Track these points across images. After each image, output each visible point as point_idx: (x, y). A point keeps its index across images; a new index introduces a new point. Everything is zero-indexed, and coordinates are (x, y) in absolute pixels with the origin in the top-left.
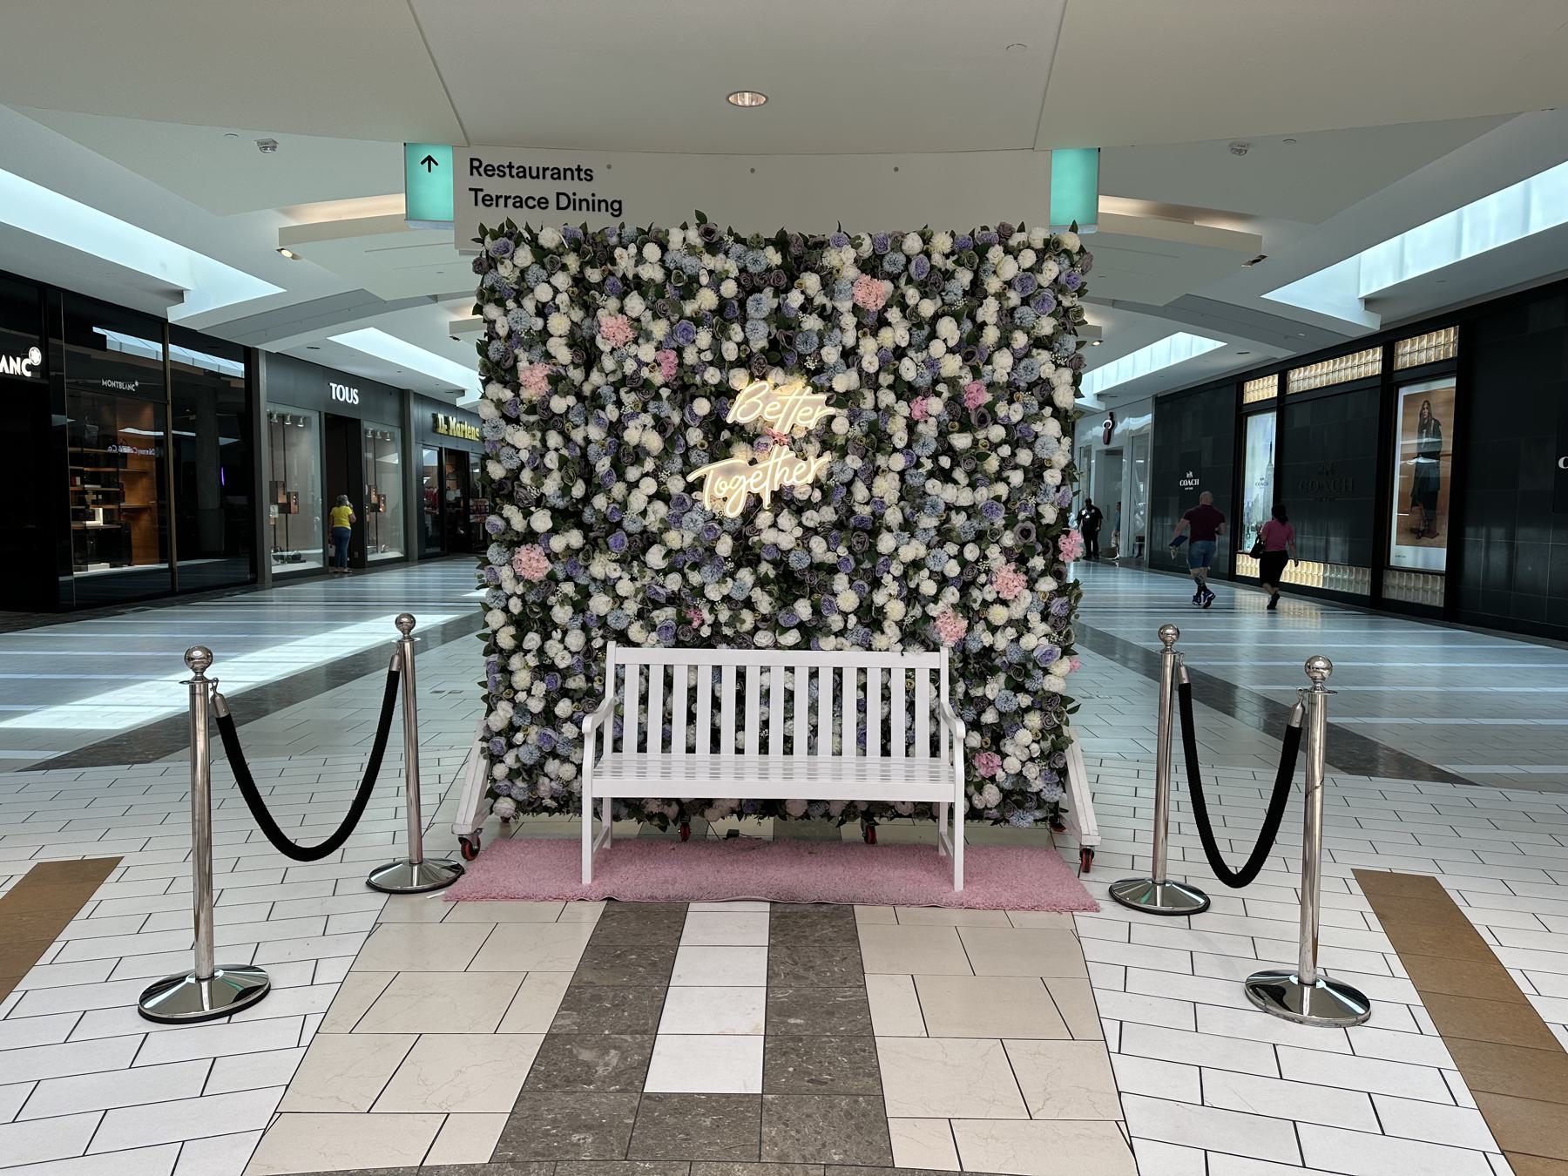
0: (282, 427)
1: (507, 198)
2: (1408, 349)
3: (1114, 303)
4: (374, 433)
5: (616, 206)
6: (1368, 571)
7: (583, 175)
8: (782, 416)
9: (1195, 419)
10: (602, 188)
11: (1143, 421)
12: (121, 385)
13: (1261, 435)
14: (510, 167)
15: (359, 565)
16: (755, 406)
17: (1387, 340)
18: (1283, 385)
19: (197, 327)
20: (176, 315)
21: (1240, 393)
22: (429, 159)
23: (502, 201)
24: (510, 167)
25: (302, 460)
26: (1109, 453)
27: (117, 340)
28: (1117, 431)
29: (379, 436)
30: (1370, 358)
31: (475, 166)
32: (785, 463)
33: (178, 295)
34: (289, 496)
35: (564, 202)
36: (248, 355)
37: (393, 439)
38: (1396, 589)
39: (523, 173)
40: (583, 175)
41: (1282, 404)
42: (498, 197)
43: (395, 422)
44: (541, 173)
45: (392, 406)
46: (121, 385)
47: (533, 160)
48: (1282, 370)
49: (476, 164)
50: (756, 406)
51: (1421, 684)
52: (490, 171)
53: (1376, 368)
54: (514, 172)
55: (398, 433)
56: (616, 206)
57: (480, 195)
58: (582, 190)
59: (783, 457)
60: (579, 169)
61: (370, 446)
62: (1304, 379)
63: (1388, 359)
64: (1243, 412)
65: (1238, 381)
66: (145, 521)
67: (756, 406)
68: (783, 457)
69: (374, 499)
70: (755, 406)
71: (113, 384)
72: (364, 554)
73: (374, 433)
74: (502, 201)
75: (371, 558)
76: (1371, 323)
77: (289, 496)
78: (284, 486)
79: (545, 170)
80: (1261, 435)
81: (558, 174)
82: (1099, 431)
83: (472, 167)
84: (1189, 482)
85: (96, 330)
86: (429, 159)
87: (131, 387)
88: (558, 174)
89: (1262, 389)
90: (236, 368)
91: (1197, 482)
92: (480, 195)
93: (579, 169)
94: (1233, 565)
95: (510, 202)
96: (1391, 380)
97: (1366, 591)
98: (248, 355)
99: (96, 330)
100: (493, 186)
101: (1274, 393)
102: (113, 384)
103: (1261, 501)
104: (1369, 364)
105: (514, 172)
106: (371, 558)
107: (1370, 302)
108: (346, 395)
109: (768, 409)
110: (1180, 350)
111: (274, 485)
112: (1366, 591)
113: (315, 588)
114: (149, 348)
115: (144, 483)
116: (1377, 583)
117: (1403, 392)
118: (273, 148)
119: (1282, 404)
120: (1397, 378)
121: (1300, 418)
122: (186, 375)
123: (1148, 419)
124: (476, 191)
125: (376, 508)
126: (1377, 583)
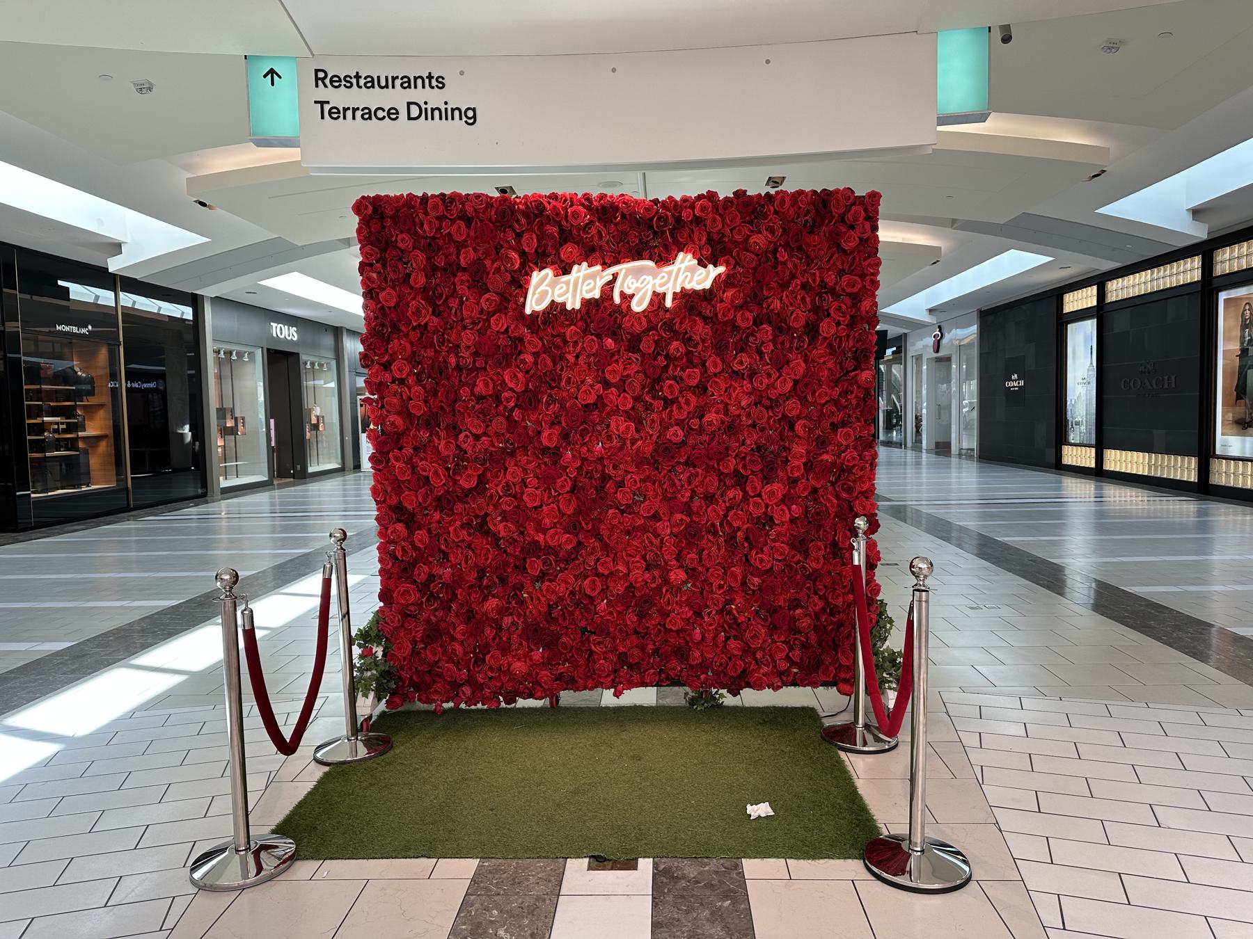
0: (228, 361)
1: (355, 110)
2: (1227, 256)
3: (953, 223)
4: (313, 364)
5: (470, 114)
6: (1194, 461)
7: (434, 83)
8: (570, 295)
9: (1019, 331)
10: (455, 96)
11: (971, 332)
12: (75, 330)
13: (1081, 343)
14: (358, 77)
15: (302, 476)
16: (545, 293)
17: (1206, 250)
18: (1101, 295)
19: (137, 276)
20: (115, 265)
21: (1060, 304)
22: (272, 72)
23: (349, 113)
24: (358, 77)
25: (252, 389)
26: (938, 360)
27: (79, 292)
28: (944, 341)
29: (317, 367)
30: (1189, 266)
31: (321, 77)
32: (687, 269)
33: (117, 248)
34: (236, 420)
35: (415, 111)
36: (195, 301)
37: (329, 369)
38: (1223, 475)
39: (371, 83)
40: (434, 83)
41: (1101, 312)
42: (345, 110)
43: (331, 355)
44: (390, 83)
45: (328, 340)
46: (75, 330)
47: (381, 71)
48: (1100, 281)
49: (321, 75)
50: (546, 293)
51: (1125, 517)
52: (336, 82)
53: (1197, 276)
54: (362, 82)
55: (334, 363)
56: (470, 114)
57: (327, 108)
58: (434, 98)
59: (687, 263)
60: (430, 77)
61: (310, 376)
62: (1118, 290)
63: (1207, 266)
64: (1063, 321)
65: (1057, 294)
66: (103, 446)
67: (546, 293)
68: (687, 263)
69: (314, 421)
70: (545, 293)
71: (67, 329)
72: (305, 468)
73: (313, 364)
74: (349, 113)
75: (311, 470)
76: (1199, 232)
77: (236, 420)
78: (232, 411)
79: (394, 79)
80: (1081, 343)
81: (407, 83)
82: (930, 341)
83: (317, 79)
84: (1015, 383)
85: (60, 283)
86: (272, 72)
87: (84, 331)
88: (407, 83)
89: (1085, 298)
90: (187, 312)
91: (1022, 383)
92: (327, 108)
93: (430, 77)
94: (1059, 455)
95: (359, 114)
96: (1209, 286)
97: (1193, 478)
98: (195, 301)
99: (60, 283)
100: (339, 97)
101: (1093, 302)
102: (67, 329)
103: (1083, 398)
104: (1189, 271)
105: (362, 82)
106: (311, 470)
107: (1197, 213)
108: (286, 333)
109: (557, 292)
110: (1012, 266)
111: (222, 413)
112: (1193, 478)
113: (262, 498)
114: (106, 297)
115: (101, 414)
116: (1204, 470)
117: (1223, 296)
118: (150, 89)
119: (1101, 312)
120: (1215, 283)
121: (1120, 324)
122: (132, 316)
123: (974, 328)
124: (322, 103)
125: (315, 427)
126: (1204, 470)
